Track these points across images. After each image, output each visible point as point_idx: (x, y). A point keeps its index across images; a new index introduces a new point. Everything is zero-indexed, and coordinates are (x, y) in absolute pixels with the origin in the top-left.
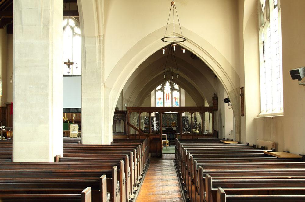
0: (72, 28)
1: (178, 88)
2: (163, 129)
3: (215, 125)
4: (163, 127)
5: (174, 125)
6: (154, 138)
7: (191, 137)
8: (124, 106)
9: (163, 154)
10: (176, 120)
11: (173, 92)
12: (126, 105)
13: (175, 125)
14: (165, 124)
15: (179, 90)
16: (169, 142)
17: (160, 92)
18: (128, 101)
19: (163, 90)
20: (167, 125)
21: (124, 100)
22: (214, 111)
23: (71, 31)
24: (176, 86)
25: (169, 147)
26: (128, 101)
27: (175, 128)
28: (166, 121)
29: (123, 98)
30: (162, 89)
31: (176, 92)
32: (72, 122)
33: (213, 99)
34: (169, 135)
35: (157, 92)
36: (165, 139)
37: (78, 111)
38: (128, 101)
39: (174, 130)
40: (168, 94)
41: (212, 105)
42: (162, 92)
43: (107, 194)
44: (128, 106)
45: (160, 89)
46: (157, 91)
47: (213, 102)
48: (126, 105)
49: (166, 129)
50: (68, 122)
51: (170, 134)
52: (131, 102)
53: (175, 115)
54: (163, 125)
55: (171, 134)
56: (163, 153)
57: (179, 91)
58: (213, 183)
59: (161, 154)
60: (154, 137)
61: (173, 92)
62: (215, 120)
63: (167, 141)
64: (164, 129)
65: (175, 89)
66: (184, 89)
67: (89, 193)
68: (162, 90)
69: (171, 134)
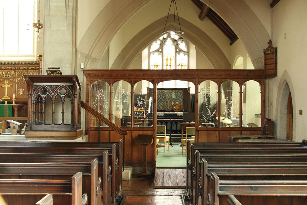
0: (174, 41)
1: (185, 49)
2: (161, 115)
3: (267, 109)
4: (158, 111)
5: (178, 107)
6: (139, 135)
7: (218, 133)
8: (78, 68)
9: (157, 170)
10: (182, 100)
11: (178, 55)
12: (82, 67)
13: (180, 108)
14: (163, 107)
15: (187, 52)
16: (170, 139)
17: (156, 54)
18: (88, 57)
19: (162, 52)
20: (167, 107)
21: (79, 56)
22: (265, 78)
23: (173, 47)
24: (183, 46)
25: (170, 147)
26: (88, 57)
27: (180, 114)
28: (166, 100)
29: (76, 51)
30: (160, 50)
31: (182, 54)
32: (13, 103)
33: (265, 53)
34: (169, 124)
35: (152, 55)
36: (162, 133)
37: (300, 114)
38: (86, 58)
39: (178, 117)
40: (169, 58)
41: (262, 66)
42: (160, 56)
43: (83, 197)
44: (88, 68)
45: (158, 51)
46: (153, 53)
47: (266, 59)
48: (82, 67)
49: (165, 114)
50: (4, 103)
51: (172, 122)
52: (94, 60)
53: (181, 91)
54: (161, 108)
55: (174, 123)
56: (159, 168)
57: (188, 53)
58: (157, 90)
59: (155, 170)
60: (141, 133)
61: (178, 55)
62: (267, 98)
63: (167, 138)
64: (162, 114)
65: (181, 51)
66: (194, 45)
67: (80, 177)
68: (160, 51)
69: (174, 123)
